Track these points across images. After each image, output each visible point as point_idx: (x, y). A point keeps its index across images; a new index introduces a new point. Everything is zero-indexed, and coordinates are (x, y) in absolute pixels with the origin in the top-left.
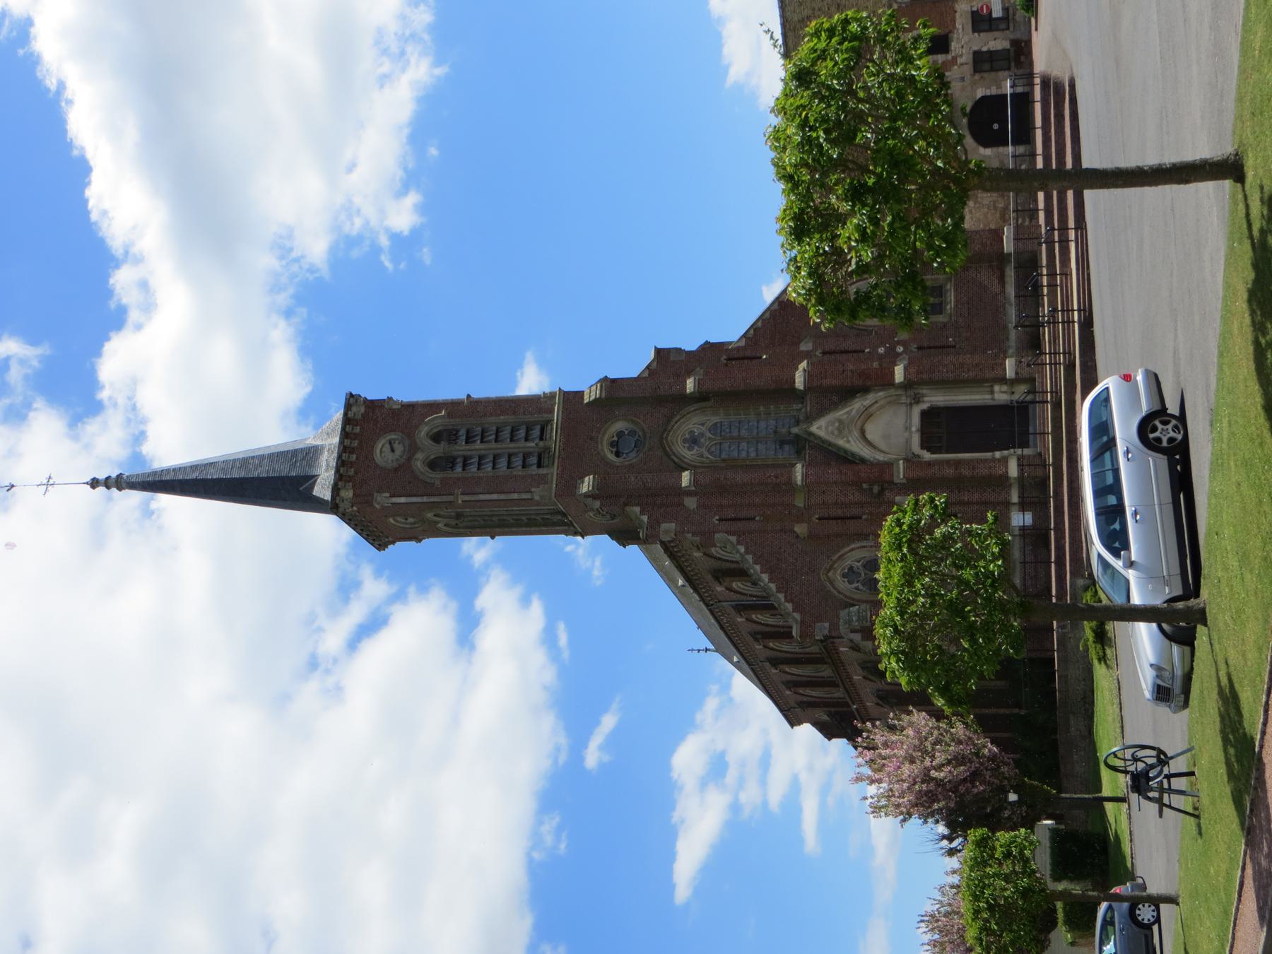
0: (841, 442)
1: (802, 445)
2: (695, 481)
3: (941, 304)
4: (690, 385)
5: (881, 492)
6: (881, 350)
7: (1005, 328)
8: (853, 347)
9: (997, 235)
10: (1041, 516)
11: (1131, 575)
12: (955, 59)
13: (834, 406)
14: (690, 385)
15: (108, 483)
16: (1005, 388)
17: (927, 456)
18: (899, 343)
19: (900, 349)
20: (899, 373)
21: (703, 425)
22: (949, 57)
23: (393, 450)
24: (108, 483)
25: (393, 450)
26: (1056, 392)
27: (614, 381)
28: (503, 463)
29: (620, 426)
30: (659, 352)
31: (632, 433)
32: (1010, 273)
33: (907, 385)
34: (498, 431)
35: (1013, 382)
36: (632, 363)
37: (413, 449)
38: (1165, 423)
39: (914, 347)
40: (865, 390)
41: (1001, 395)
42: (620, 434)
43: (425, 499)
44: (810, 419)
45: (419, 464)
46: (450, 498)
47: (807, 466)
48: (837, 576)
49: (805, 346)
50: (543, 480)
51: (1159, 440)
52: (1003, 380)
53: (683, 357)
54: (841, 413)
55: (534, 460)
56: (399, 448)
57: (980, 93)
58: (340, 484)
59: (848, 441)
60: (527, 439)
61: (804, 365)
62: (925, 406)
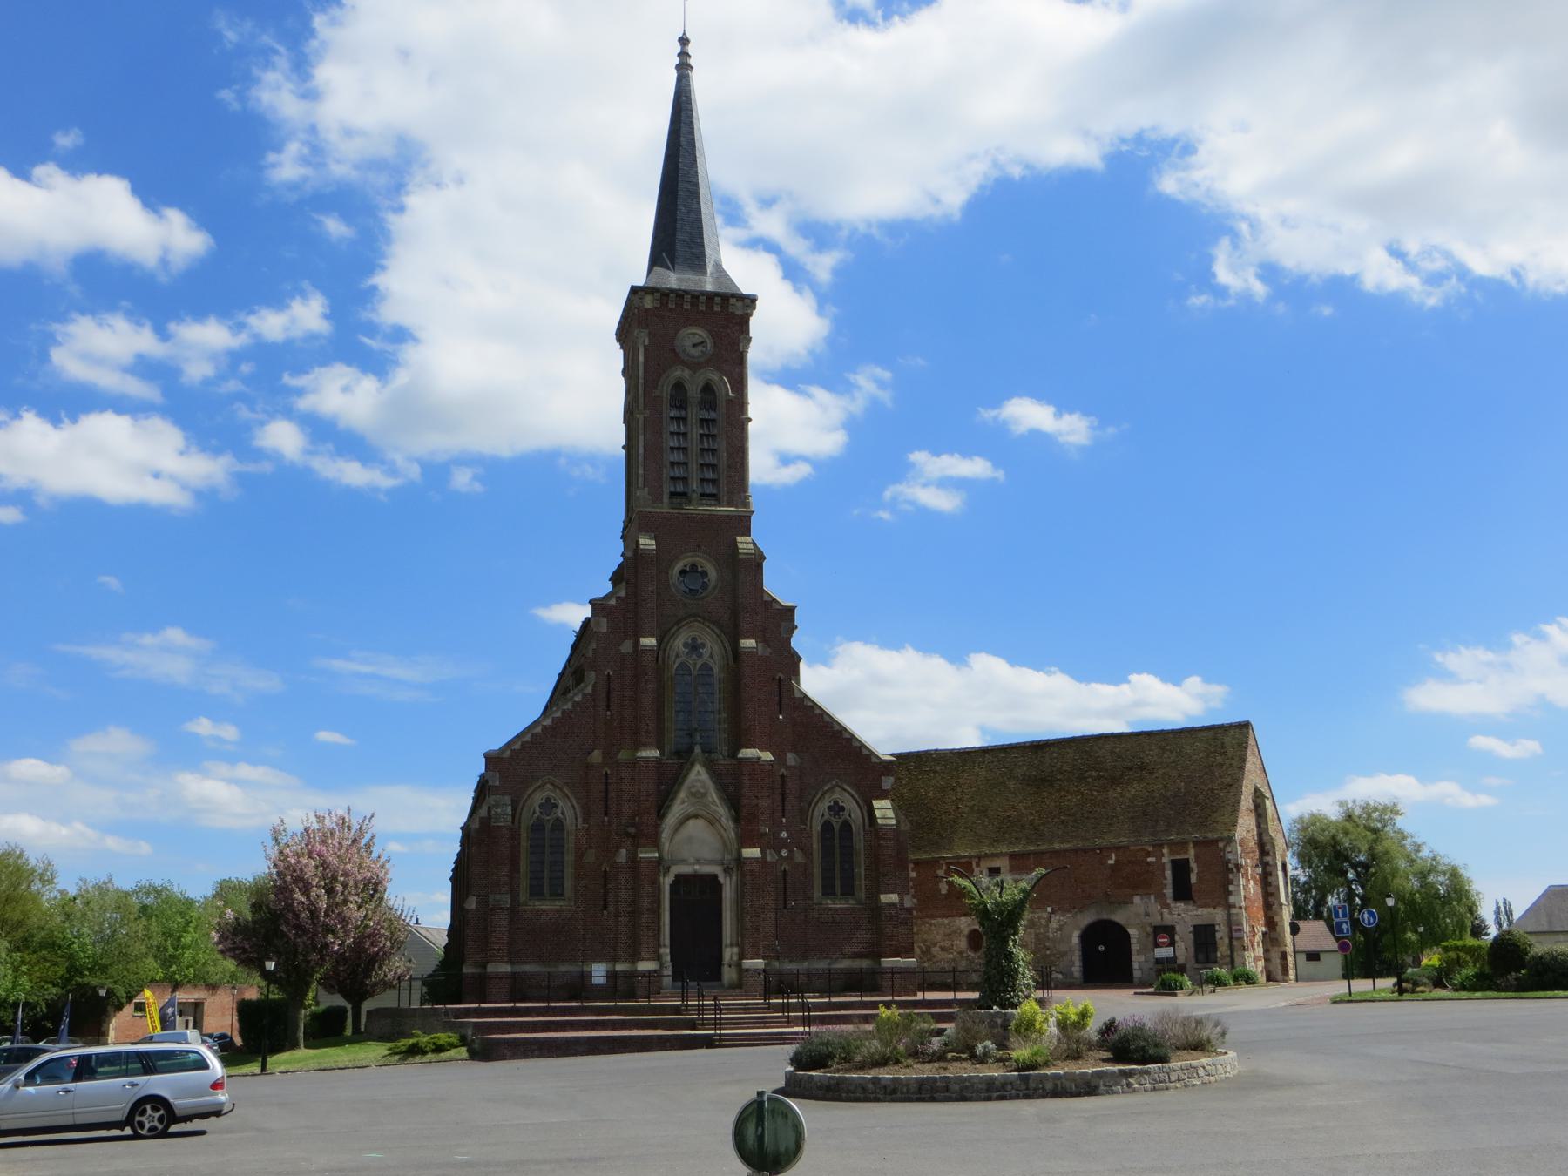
0: (682, 795)
1: (683, 757)
2: (647, 650)
3: (834, 894)
4: (748, 643)
5: (628, 835)
6: (784, 834)
7: (805, 958)
9: (908, 951)
10: (600, 993)
11: (8, 1086)
12: (1167, 906)
13: (722, 787)
14: (748, 643)
15: (684, 55)
16: (735, 958)
17: (667, 882)
18: (791, 852)
19: (784, 853)
20: (753, 853)
21: (711, 657)
23: (694, 346)
24: (684, 55)
25: (694, 346)
26: (687, 1009)
27: (760, 566)
28: (677, 457)
29: (713, 574)
30: (791, 610)
31: (705, 586)
32: (865, 964)
33: (740, 861)
34: (714, 451)
35: (739, 965)
36: (777, 584)
37: (695, 366)
38: (160, 1119)
39: (786, 867)
40: (736, 820)
41: (729, 954)
42: (704, 574)
43: (641, 381)
44: (710, 766)
45: (679, 373)
46: (641, 406)
47: (659, 762)
48: (548, 792)
49: (791, 758)
50: (657, 499)
51: (143, 1113)
52: (742, 956)
54: (713, 795)
55: (680, 488)
56: (696, 352)
57: (1132, 932)
58: (658, 295)
60: (702, 480)
61: (767, 756)
62: (721, 878)
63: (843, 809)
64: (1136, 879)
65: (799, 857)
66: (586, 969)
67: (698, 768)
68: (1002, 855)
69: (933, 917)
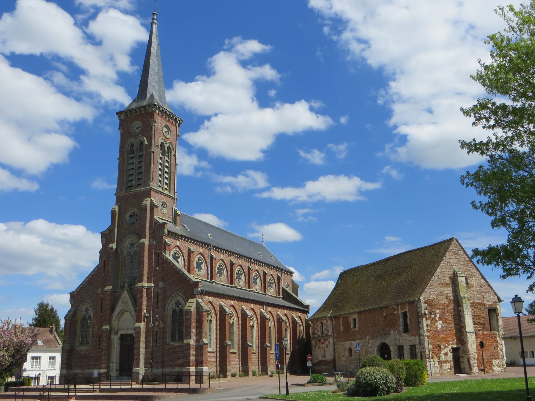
8: (159, 304)
18: (159, 323)
22: (402, 333)
37: (135, 137)
44: (127, 291)
49: (161, 284)
53: (104, 239)
57: (391, 348)
59: (120, 305)
63: (180, 304)
64: (391, 324)
65: (162, 325)
66: (92, 372)
67: (126, 292)
68: (354, 313)
69: (339, 342)
